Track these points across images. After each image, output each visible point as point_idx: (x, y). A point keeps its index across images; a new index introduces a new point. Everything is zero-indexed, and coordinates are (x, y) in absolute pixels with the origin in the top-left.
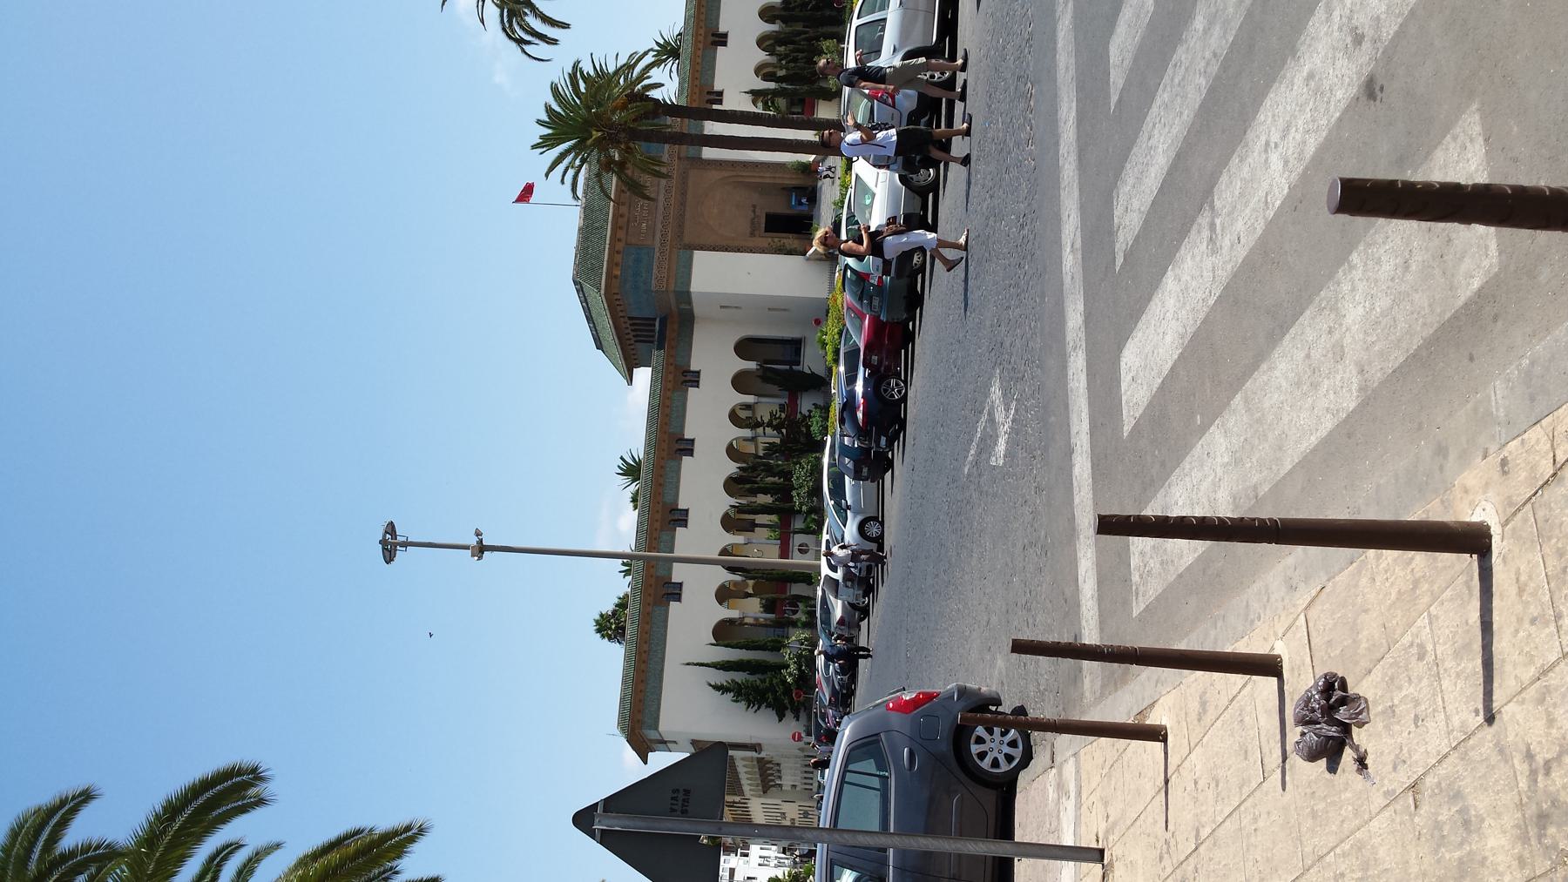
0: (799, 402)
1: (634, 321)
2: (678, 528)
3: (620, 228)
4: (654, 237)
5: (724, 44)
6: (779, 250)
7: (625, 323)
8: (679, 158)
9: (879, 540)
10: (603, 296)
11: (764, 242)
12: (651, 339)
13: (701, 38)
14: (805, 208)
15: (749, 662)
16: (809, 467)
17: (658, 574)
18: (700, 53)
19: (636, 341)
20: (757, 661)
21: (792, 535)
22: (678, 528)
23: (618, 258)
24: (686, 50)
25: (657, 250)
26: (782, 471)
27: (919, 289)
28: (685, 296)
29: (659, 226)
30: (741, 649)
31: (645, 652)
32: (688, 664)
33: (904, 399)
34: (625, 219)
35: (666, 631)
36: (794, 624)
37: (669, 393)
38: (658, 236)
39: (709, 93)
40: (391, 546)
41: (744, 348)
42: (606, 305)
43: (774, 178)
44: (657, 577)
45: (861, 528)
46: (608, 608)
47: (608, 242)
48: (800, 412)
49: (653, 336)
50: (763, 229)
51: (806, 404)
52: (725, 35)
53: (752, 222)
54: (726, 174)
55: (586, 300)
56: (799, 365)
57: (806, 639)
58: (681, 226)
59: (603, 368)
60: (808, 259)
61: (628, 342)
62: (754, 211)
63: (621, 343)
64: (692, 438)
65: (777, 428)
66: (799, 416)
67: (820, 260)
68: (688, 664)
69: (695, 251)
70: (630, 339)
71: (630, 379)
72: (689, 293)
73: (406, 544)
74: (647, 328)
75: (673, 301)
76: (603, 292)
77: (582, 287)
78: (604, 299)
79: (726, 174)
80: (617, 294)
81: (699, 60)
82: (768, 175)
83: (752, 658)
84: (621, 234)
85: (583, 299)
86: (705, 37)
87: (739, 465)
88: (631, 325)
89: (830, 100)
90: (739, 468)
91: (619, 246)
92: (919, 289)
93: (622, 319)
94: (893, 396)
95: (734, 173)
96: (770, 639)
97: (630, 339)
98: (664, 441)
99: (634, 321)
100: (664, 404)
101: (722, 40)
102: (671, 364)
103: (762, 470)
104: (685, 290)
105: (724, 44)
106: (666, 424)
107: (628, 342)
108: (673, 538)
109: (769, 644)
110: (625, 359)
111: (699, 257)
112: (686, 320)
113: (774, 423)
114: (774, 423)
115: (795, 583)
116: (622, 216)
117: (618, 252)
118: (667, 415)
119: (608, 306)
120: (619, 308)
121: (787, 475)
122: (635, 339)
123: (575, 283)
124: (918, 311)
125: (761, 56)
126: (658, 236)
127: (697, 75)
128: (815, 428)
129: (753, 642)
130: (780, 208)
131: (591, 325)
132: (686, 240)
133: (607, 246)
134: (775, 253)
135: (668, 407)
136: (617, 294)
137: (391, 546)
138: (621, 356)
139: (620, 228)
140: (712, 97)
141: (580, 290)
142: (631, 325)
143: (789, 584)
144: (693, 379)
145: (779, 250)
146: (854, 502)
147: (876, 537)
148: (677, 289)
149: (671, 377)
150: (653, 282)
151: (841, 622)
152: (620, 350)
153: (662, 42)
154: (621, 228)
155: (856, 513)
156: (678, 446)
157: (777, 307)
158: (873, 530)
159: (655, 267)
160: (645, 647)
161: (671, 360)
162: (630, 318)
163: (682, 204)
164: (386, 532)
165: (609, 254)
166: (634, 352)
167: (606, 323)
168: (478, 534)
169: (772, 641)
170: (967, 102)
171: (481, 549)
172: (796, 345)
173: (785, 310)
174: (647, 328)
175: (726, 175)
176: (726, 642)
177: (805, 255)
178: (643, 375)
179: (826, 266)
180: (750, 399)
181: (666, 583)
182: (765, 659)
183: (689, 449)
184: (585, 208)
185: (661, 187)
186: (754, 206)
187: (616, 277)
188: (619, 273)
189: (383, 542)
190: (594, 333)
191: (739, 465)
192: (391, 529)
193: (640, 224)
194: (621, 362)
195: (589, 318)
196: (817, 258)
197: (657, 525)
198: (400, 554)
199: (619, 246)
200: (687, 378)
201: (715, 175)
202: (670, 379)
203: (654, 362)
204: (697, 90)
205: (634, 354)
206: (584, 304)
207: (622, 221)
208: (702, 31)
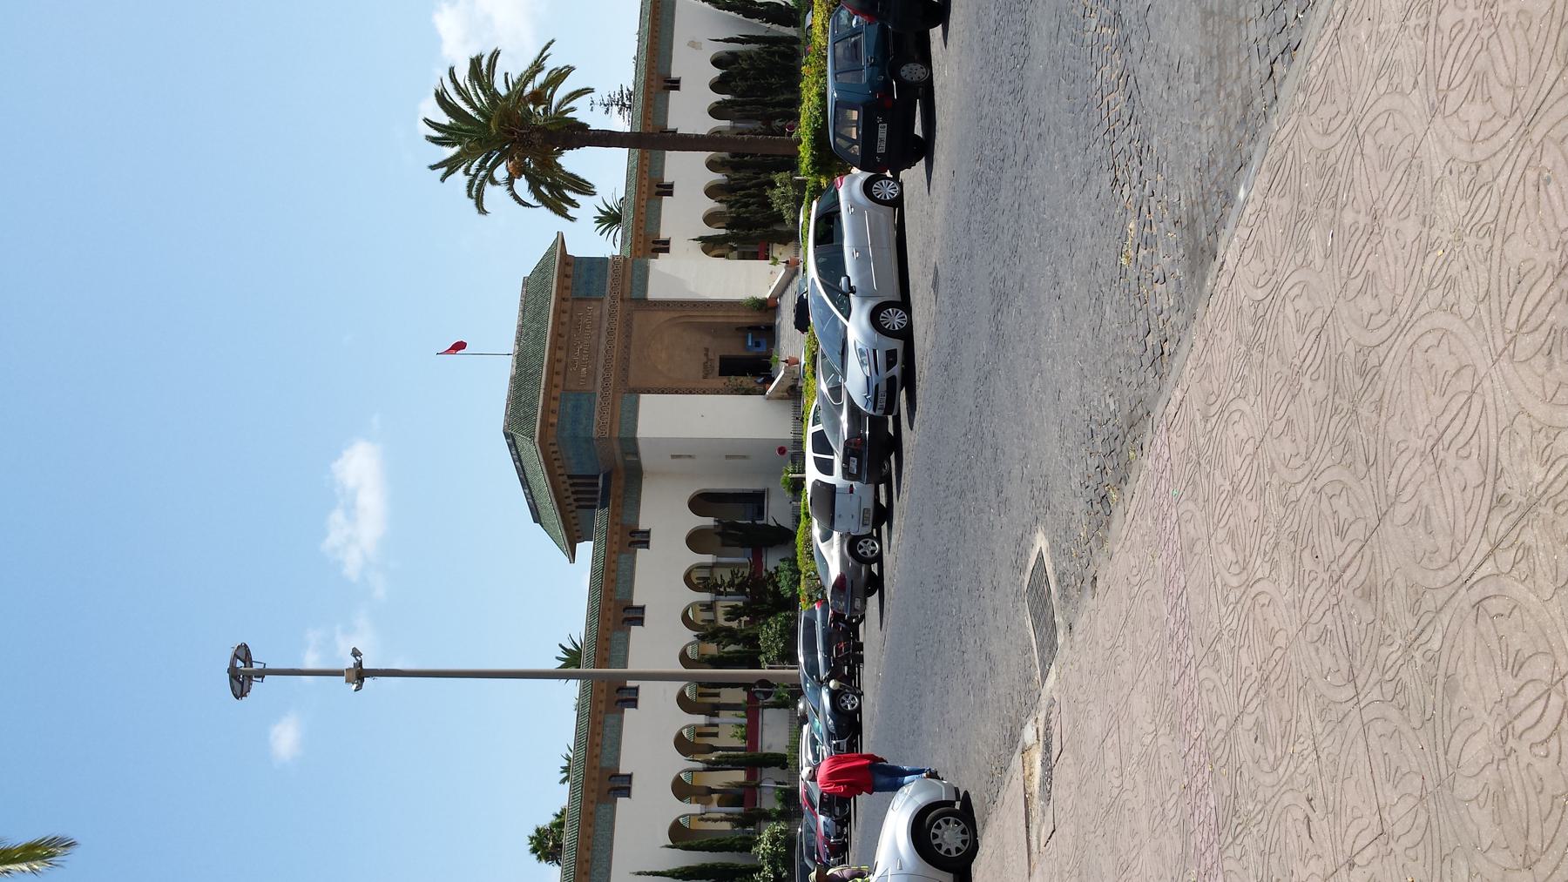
0: (764, 560)
1: (575, 481)
2: (626, 709)
3: (557, 373)
4: (595, 379)
5: (670, 194)
6: (736, 390)
7: (564, 482)
8: (622, 300)
9: (906, 335)
10: (537, 445)
11: (721, 382)
12: (594, 496)
13: (644, 189)
14: (763, 349)
15: (713, 866)
16: (778, 627)
17: (604, 765)
18: (643, 203)
19: (577, 507)
20: (723, 865)
21: (760, 710)
22: (626, 709)
23: (554, 405)
24: (629, 217)
25: (598, 395)
26: (747, 637)
27: (891, 430)
28: (630, 444)
29: (601, 370)
30: (704, 851)
31: (587, 861)
32: (639, 874)
33: (859, 710)
34: (563, 363)
35: (612, 834)
36: (767, 817)
37: (614, 557)
38: (600, 380)
39: (654, 242)
40: (243, 675)
41: (701, 503)
42: (540, 456)
43: (728, 316)
44: (602, 770)
45: (875, 317)
46: (546, 820)
47: (543, 386)
48: (766, 570)
49: (596, 492)
50: (717, 369)
51: (772, 561)
52: (671, 186)
53: (705, 365)
54: (676, 315)
55: (519, 456)
56: (763, 519)
57: (782, 832)
58: (625, 370)
59: (541, 544)
60: (769, 398)
61: (569, 508)
62: (706, 355)
63: (560, 508)
64: (642, 604)
65: (740, 589)
66: (764, 574)
67: (782, 398)
68: (639, 874)
69: (642, 395)
70: (570, 504)
71: (572, 555)
72: (634, 440)
73: (262, 674)
74: (587, 496)
75: (618, 452)
76: (536, 440)
77: (514, 440)
78: (538, 448)
79: (676, 315)
80: (554, 444)
81: (643, 210)
82: (720, 314)
83: (717, 862)
84: (558, 380)
85: (516, 457)
86: (649, 189)
87: (696, 633)
88: (571, 485)
89: (786, 244)
90: (697, 636)
91: (556, 393)
92: (891, 430)
93: (561, 478)
94: (847, 707)
95: (683, 314)
96: (738, 836)
97: (570, 504)
98: (609, 610)
99: (575, 481)
100: (608, 569)
101: (675, 85)
102: (617, 524)
103: (724, 637)
104: (630, 436)
105: (670, 194)
106: (611, 590)
107: (569, 508)
108: (621, 720)
109: (736, 843)
110: (566, 529)
111: (645, 400)
112: (634, 475)
113: (736, 582)
114: (736, 582)
115: (766, 767)
116: (559, 361)
117: (555, 399)
118: (612, 581)
119: (544, 459)
120: (557, 464)
121: (752, 640)
122: (573, 489)
123: (507, 436)
124: (893, 457)
125: (711, 204)
126: (600, 380)
127: (642, 225)
128: (784, 585)
129: (718, 840)
130: (734, 348)
131: (527, 491)
132: (632, 383)
133: (542, 391)
134: (732, 393)
135: (613, 571)
136: (554, 444)
137: (243, 675)
138: (561, 524)
139: (557, 373)
140: (658, 246)
141: (513, 446)
142: (573, 493)
143: (759, 769)
144: (642, 539)
145: (736, 390)
146: (861, 281)
147: (900, 330)
148: (621, 435)
149: (616, 538)
150: (594, 429)
151: (840, 584)
152: (559, 517)
153: (606, 209)
154: (557, 373)
155: (865, 297)
156: (626, 615)
157: (735, 453)
158: (895, 319)
159: (596, 413)
160: (587, 855)
161: (616, 520)
162: (570, 477)
163: (626, 347)
164: (236, 656)
165: (544, 400)
166: (577, 528)
167: (541, 482)
168: (356, 653)
169: (741, 838)
170: (895, 522)
171: (359, 675)
172: (756, 500)
173: (744, 457)
174: (587, 496)
175: (677, 315)
176: (685, 843)
177: (763, 393)
178: (585, 549)
179: (790, 403)
180: (708, 559)
181: (612, 776)
182: (731, 862)
183: (636, 618)
184: (518, 356)
185: (602, 329)
186: (707, 350)
187: (552, 425)
188: (556, 421)
189: (234, 673)
190: (531, 501)
191: (696, 633)
192: (243, 653)
193: (579, 369)
194: (560, 532)
195: (525, 482)
196: (778, 397)
197: (602, 707)
198: (256, 686)
199: (556, 393)
200: (636, 539)
201: (663, 316)
202: (614, 549)
203: (596, 535)
204: (641, 239)
205: (576, 525)
206: (518, 464)
207: (559, 367)
208: (646, 183)
